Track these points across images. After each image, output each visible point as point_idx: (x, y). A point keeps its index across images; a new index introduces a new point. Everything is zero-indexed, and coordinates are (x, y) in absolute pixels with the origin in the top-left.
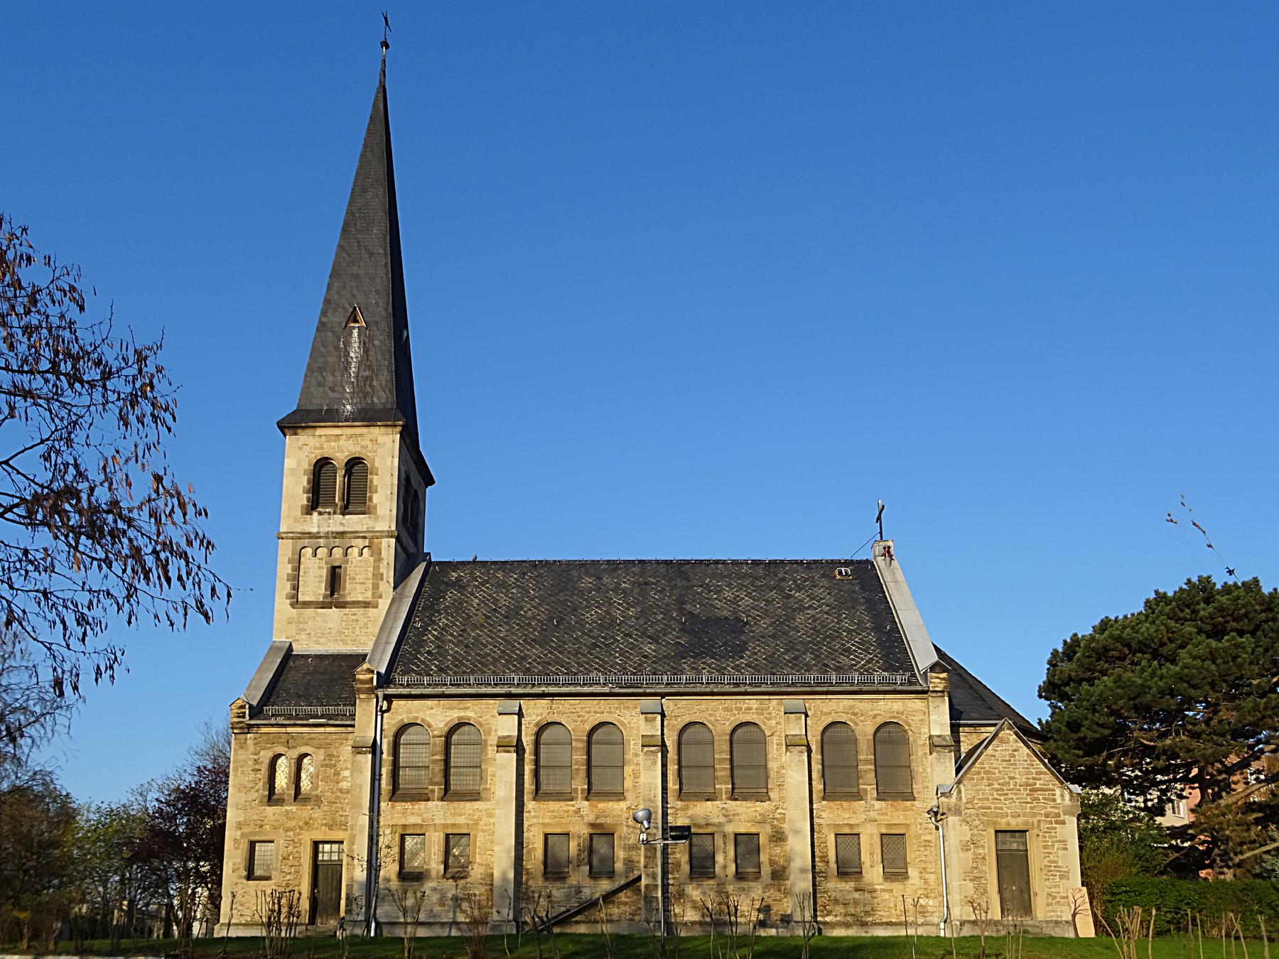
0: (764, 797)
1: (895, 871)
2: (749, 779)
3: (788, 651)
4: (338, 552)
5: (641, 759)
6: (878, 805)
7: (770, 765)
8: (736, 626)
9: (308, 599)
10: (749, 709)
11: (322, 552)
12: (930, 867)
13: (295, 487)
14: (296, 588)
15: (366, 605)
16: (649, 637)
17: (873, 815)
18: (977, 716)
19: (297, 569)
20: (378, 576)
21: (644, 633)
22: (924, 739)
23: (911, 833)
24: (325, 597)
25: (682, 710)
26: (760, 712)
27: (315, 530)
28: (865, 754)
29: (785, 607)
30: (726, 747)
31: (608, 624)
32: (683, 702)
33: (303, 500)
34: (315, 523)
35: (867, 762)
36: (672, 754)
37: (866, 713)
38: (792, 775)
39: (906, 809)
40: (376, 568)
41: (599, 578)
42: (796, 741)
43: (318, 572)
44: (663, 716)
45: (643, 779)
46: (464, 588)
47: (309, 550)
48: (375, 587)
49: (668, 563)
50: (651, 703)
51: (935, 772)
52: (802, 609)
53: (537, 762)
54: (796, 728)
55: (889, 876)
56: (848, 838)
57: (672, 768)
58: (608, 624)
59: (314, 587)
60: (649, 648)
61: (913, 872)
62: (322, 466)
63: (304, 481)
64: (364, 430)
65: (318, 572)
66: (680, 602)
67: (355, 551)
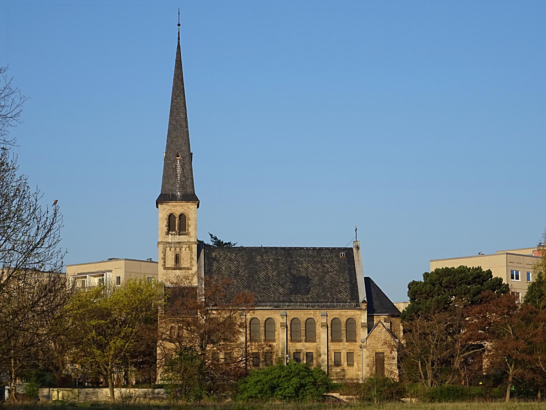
0: (315, 341)
1: (351, 364)
2: (311, 337)
3: (323, 291)
4: (178, 249)
5: (280, 329)
6: (346, 343)
7: (317, 331)
8: (307, 280)
9: (169, 266)
10: (311, 313)
11: (173, 249)
12: (360, 362)
13: (163, 225)
14: (165, 262)
15: (188, 269)
16: (281, 285)
17: (345, 346)
18: (379, 311)
19: (165, 255)
20: (192, 259)
21: (279, 284)
22: (360, 324)
23: (355, 352)
24: (174, 265)
25: (292, 314)
26: (314, 314)
27: (170, 241)
28: (343, 328)
29: (323, 272)
30: (304, 326)
31: (267, 279)
32: (292, 311)
33: (166, 229)
34: (170, 239)
35: (344, 330)
36: (289, 328)
37: (344, 314)
38: (322, 334)
39: (354, 345)
40: (191, 255)
41: (262, 257)
42: (324, 324)
43: (172, 256)
44: (286, 316)
45: (281, 336)
46: (218, 261)
47: (168, 248)
48: (191, 262)
49: (284, 249)
50: (283, 312)
51: (362, 333)
52: (328, 272)
53: (250, 330)
54: (324, 321)
55: (348, 365)
56: (338, 354)
57: (289, 332)
58: (267, 279)
59: (171, 263)
60: (281, 290)
61: (355, 364)
62: (171, 217)
63: (166, 223)
64: (185, 204)
65: (172, 256)
66: (290, 269)
67: (184, 249)
